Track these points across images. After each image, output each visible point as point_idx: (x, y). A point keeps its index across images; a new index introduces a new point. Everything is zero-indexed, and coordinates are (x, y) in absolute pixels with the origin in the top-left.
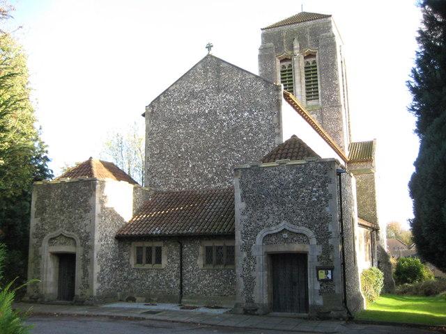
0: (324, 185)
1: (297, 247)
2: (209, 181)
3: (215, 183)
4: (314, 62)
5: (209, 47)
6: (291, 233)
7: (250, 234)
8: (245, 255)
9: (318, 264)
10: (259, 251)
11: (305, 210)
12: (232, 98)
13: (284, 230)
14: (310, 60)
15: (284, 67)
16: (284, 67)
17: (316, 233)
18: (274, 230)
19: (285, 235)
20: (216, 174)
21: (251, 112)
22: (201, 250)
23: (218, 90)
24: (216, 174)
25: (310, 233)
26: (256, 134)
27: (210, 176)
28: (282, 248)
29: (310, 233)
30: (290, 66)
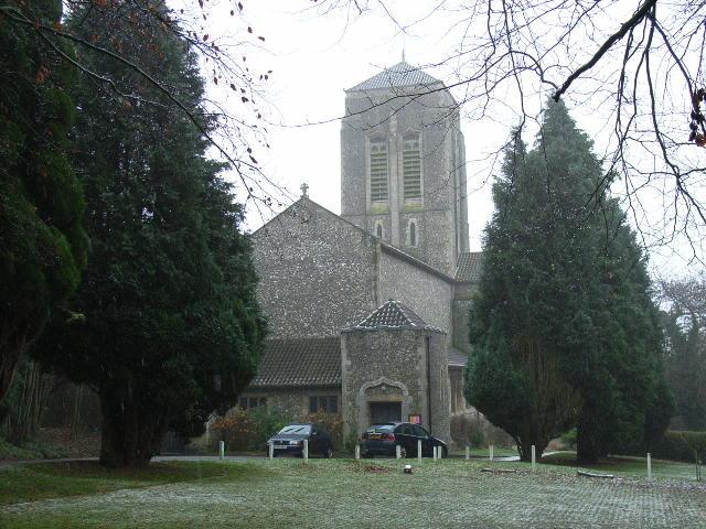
0: (415, 349)
1: (393, 398)
2: (305, 330)
3: (311, 332)
4: (416, 145)
5: (305, 188)
6: (388, 386)
7: (354, 387)
8: (350, 404)
9: (410, 412)
10: (362, 402)
11: (400, 368)
12: (329, 246)
13: (383, 384)
14: (411, 142)
15: (374, 148)
16: (374, 148)
17: (408, 386)
18: (375, 383)
19: (384, 388)
20: (312, 323)
21: (348, 264)
22: (306, 400)
23: (315, 237)
24: (312, 323)
25: (404, 387)
26: (354, 285)
27: (306, 325)
28: (380, 398)
29: (404, 387)
30: (383, 148)
